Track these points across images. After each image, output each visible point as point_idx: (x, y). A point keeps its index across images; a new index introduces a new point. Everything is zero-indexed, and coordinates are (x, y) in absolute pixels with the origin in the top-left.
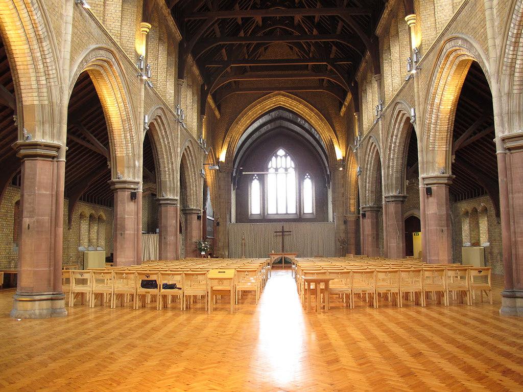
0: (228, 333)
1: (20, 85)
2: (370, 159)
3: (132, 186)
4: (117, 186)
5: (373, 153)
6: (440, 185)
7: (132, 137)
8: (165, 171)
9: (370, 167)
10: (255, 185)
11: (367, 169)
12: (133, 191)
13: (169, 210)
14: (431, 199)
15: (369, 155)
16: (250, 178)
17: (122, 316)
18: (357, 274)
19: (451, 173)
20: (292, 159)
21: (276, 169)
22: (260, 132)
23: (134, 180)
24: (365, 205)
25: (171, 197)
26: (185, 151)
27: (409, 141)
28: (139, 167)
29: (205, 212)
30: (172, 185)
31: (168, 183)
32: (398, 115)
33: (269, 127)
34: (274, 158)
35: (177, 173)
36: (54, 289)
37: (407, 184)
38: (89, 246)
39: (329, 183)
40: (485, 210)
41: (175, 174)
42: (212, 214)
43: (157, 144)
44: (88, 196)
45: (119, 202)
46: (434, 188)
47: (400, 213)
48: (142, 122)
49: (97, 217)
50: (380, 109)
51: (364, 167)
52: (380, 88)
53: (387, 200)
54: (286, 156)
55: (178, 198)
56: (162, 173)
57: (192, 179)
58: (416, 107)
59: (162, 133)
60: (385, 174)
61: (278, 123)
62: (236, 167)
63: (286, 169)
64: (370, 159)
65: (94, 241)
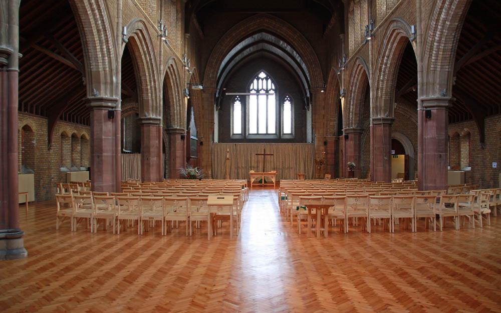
0: (219, 288)
1: (88, 52)
2: (355, 81)
3: (110, 104)
4: (93, 104)
5: (358, 75)
6: (440, 108)
7: (108, 49)
8: (147, 90)
9: (355, 90)
10: (237, 106)
11: (351, 91)
12: (110, 109)
13: (151, 130)
14: (430, 123)
15: (354, 77)
16: (232, 100)
17: (104, 239)
18: (351, 199)
19: (451, 96)
20: (272, 82)
21: (258, 91)
22: (243, 54)
23: (111, 98)
24: (349, 126)
25: (154, 117)
26: (168, 70)
27: (400, 63)
28: (117, 83)
29: (188, 133)
30: (154, 104)
31: (150, 102)
32: (392, 35)
33: (251, 49)
34: (255, 81)
35: (160, 91)
36: (10, 226)
37: (395, 107)
38: (72, 166)
39: (308, 105)
40: (468, 135)
41: (158, 91)
42: (195, 133)
43: (139, 61)
44: (69, 115)
45: (95, 122)
46: (434, 111)
47: (388, 136)
48: (120, 35)
49: (79, 136)
50: (370, 29)
51: (348, 89)
52: (371, 8)
53: (375, 123)
54: (267, 79)
55: (161, 118)
56: (145, 91)
57: (176, 99)
58: (418, 24)
59: (143, 49)
60: (373, 95)
61: (260, 46)
62: (219, 87)
63: (267, 91)
64: (355, 81)
65: (78, 161)
